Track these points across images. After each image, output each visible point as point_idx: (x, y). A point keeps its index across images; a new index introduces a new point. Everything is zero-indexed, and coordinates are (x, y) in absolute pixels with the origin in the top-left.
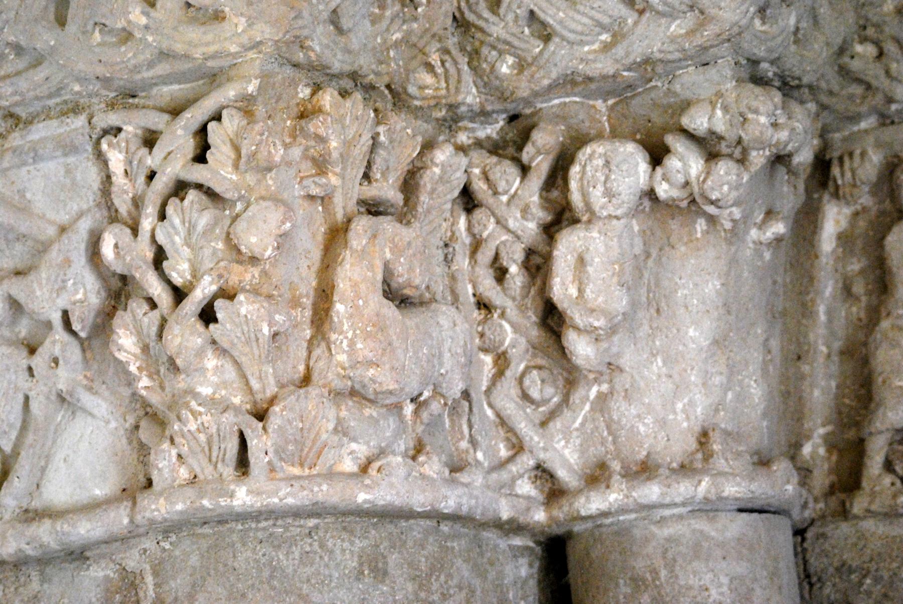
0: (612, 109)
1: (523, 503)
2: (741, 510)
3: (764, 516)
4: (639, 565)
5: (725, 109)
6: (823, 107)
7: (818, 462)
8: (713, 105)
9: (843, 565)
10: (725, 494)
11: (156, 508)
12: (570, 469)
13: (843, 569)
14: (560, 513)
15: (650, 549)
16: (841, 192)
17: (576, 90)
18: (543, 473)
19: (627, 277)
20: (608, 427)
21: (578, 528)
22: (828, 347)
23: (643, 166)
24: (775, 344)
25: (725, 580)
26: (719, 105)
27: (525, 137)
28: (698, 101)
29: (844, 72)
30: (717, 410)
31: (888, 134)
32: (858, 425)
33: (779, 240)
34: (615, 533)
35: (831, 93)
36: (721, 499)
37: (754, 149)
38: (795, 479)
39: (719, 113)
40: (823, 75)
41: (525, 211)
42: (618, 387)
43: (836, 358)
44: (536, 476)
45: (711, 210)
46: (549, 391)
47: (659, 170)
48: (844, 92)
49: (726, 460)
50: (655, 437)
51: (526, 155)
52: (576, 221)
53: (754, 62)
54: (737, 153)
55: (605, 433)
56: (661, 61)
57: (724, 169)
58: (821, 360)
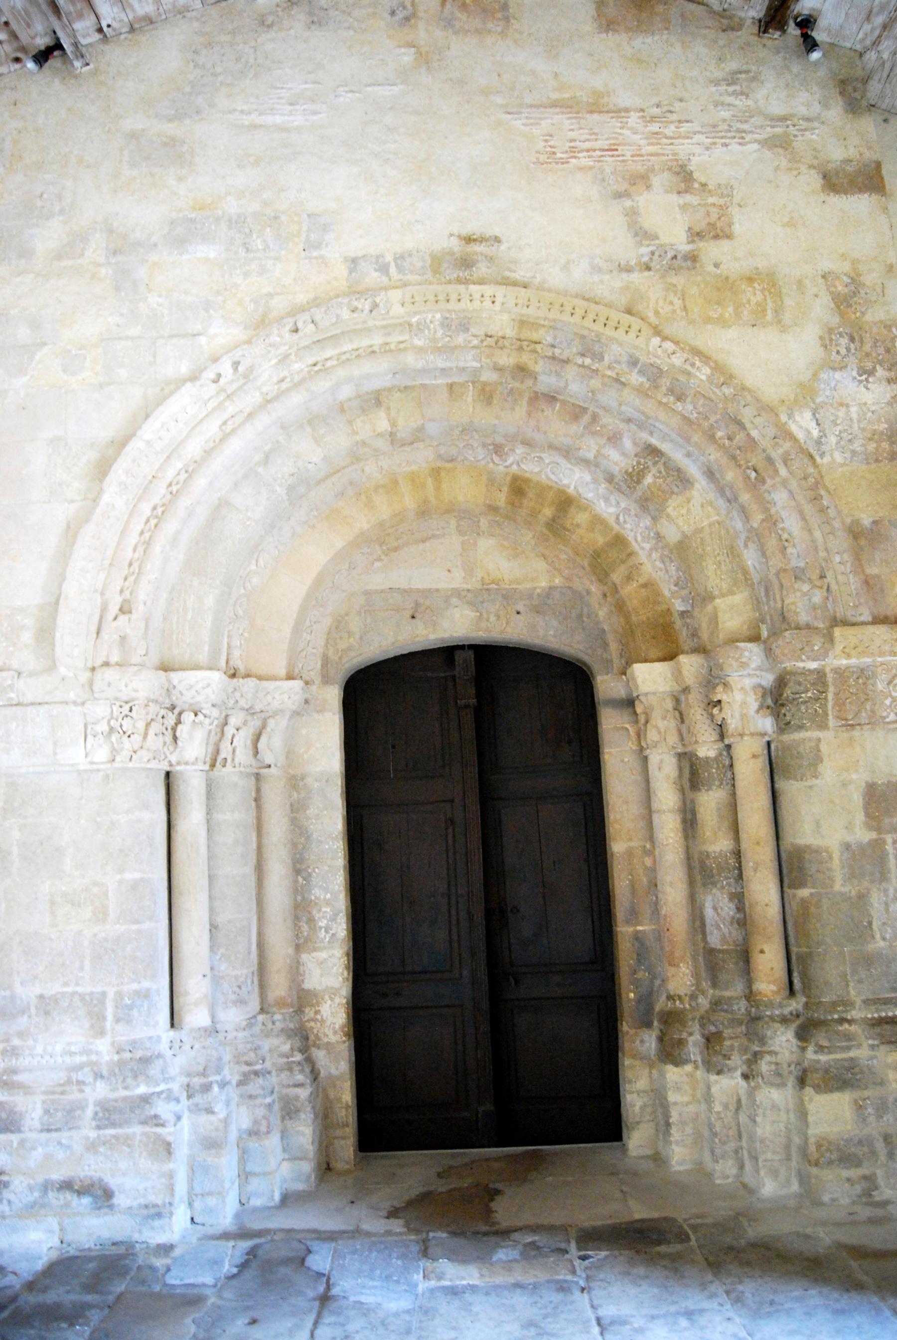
11: (116, 765)
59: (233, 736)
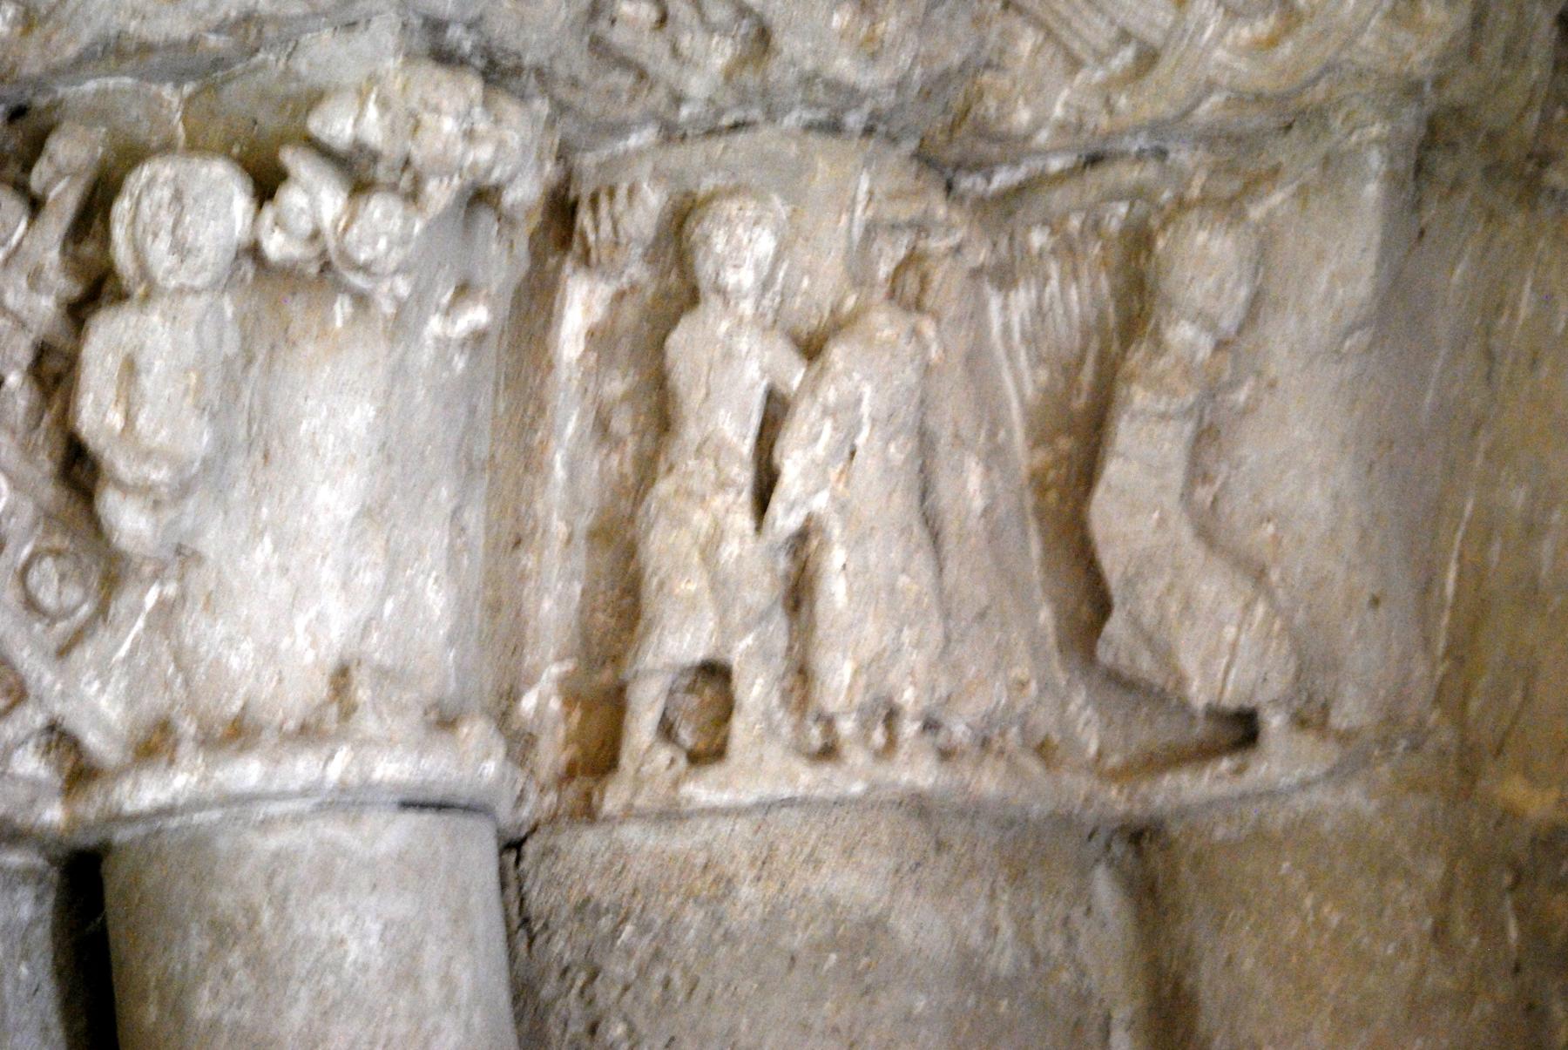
0: (189, 101)
1: (22, 794)
2: (406, 805)
3: (445, 817)
4: (226, 900)
5: (384, 104)
6: (561, 108)
7: (549, 725)
8: (362, 96)
9: (587, 901)
10: (377, 775)
12: (108, 730)
13: (586, 909)
14: (91, 807)
15: (245, 871)
16: (593, 255)
17: (127, 65)
18: (59, 739)
19: (212, 395)
20: (177, 659)
21: (121, 835)
22: (569, 523)
23: (240, 202)
24: (473, 518)
25: (375, 927)
26: (373, 96)
27: (36, 146)
28: (338, 89)
29: (598, 46)
30: (365, 632)
31: (676, 157)
32: (617, 660)
33: (478, 338)
34: (183, 844)
35: (574, 83)
36: (367, 785)
37: (433, 173)
38: (500, 751)
39: (372, 112)
40: (560, 52)
41: (35, 279)
42: (194, 588)
43: (581, 543)
44: (49, 744)
45: (358, 281)
46: (73, 594)
47: (268, 213)
48: (600, 83)
49: (380, 716)
50: (258, 676)
51: (39, 177)
52: (122, 296)
53: (436, 26)
54: (405, 182)
55: (171, 670)
56: (274, 19)
57: (380, 210)
58: (556, 546)
59: (775, 415)
